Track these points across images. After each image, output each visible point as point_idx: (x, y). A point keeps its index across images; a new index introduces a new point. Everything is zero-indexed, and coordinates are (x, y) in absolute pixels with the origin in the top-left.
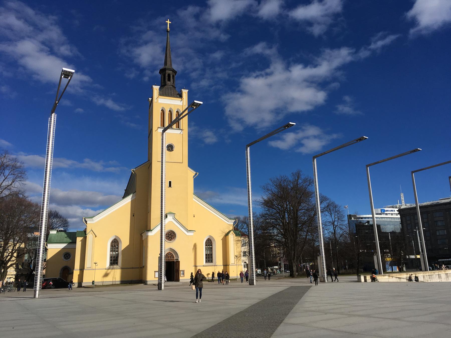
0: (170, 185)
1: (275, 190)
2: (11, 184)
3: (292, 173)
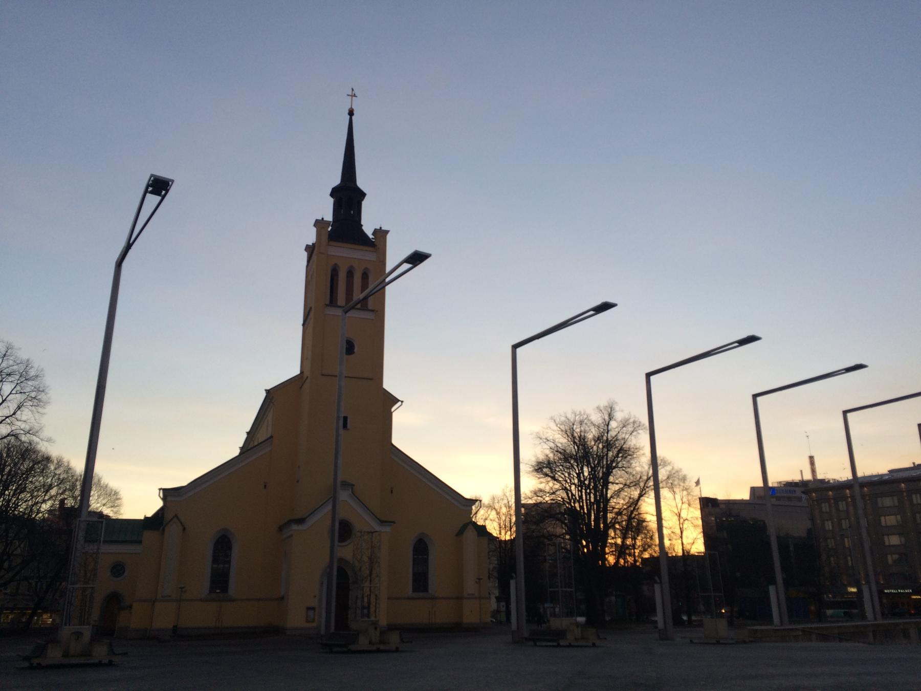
1: (562, 441)
2: (14, 414)
3: (598, 408)
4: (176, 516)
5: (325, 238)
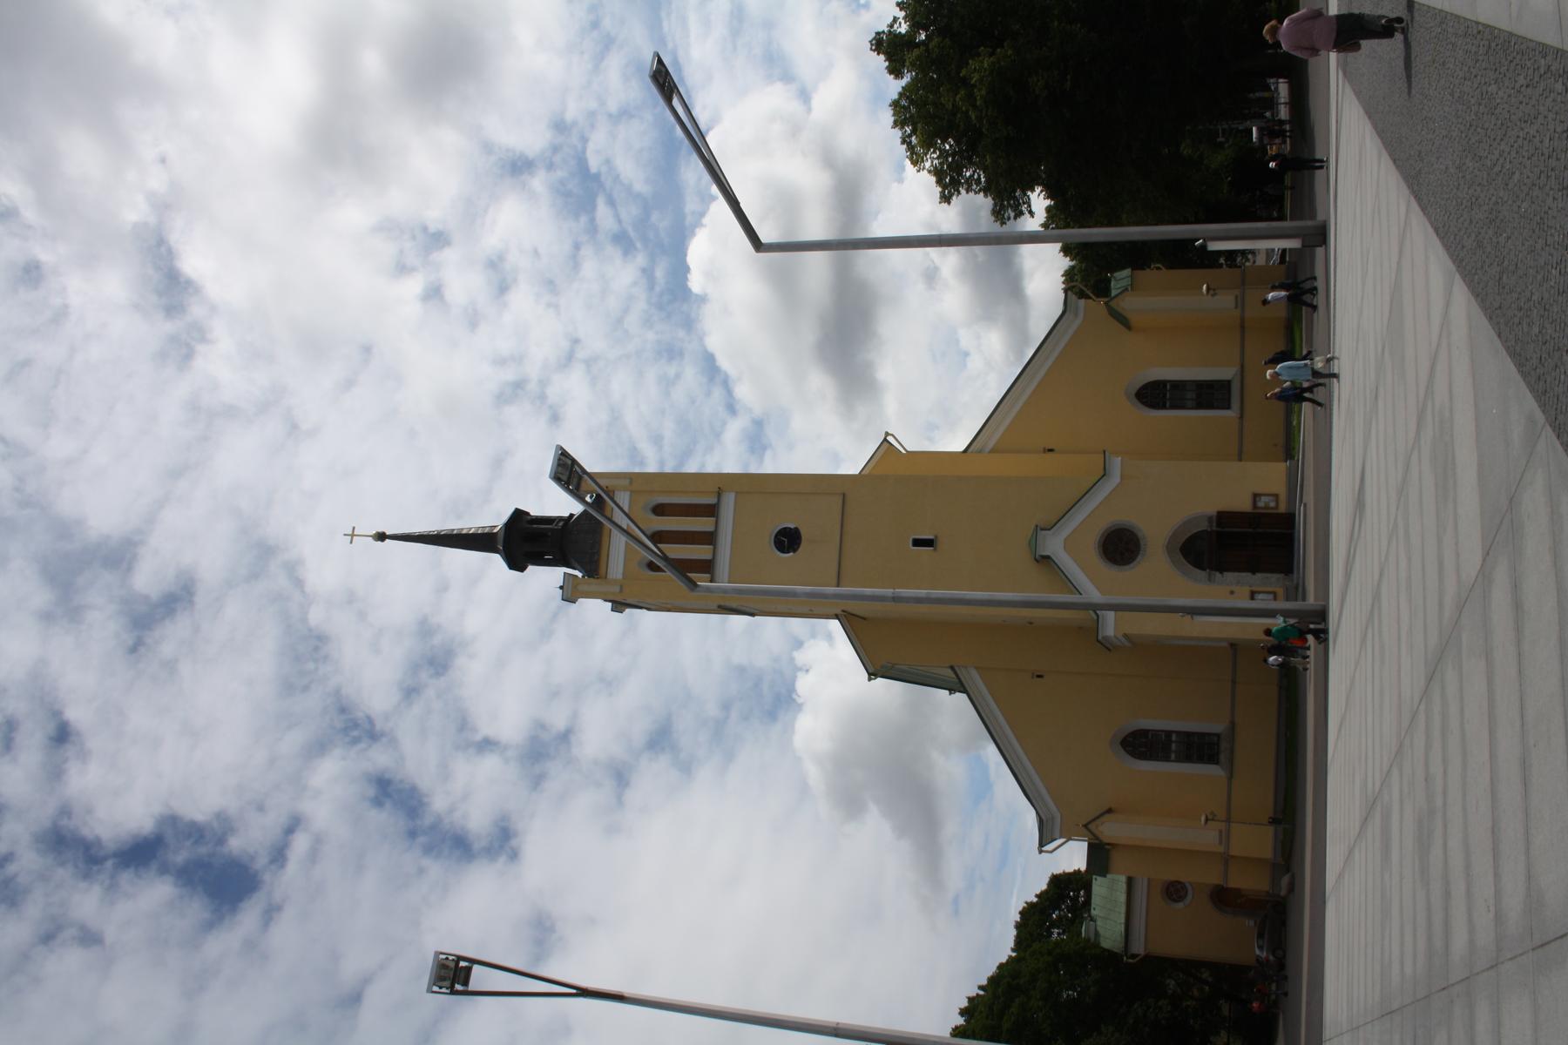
0: (928, 543)
4: (1085, 826)
5: (593, 584)
